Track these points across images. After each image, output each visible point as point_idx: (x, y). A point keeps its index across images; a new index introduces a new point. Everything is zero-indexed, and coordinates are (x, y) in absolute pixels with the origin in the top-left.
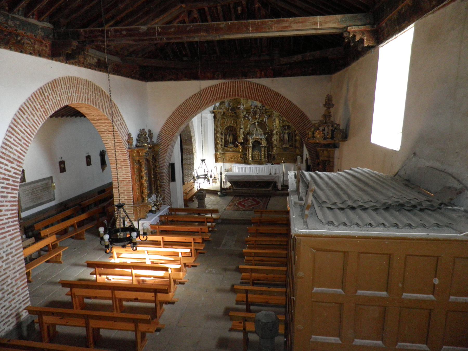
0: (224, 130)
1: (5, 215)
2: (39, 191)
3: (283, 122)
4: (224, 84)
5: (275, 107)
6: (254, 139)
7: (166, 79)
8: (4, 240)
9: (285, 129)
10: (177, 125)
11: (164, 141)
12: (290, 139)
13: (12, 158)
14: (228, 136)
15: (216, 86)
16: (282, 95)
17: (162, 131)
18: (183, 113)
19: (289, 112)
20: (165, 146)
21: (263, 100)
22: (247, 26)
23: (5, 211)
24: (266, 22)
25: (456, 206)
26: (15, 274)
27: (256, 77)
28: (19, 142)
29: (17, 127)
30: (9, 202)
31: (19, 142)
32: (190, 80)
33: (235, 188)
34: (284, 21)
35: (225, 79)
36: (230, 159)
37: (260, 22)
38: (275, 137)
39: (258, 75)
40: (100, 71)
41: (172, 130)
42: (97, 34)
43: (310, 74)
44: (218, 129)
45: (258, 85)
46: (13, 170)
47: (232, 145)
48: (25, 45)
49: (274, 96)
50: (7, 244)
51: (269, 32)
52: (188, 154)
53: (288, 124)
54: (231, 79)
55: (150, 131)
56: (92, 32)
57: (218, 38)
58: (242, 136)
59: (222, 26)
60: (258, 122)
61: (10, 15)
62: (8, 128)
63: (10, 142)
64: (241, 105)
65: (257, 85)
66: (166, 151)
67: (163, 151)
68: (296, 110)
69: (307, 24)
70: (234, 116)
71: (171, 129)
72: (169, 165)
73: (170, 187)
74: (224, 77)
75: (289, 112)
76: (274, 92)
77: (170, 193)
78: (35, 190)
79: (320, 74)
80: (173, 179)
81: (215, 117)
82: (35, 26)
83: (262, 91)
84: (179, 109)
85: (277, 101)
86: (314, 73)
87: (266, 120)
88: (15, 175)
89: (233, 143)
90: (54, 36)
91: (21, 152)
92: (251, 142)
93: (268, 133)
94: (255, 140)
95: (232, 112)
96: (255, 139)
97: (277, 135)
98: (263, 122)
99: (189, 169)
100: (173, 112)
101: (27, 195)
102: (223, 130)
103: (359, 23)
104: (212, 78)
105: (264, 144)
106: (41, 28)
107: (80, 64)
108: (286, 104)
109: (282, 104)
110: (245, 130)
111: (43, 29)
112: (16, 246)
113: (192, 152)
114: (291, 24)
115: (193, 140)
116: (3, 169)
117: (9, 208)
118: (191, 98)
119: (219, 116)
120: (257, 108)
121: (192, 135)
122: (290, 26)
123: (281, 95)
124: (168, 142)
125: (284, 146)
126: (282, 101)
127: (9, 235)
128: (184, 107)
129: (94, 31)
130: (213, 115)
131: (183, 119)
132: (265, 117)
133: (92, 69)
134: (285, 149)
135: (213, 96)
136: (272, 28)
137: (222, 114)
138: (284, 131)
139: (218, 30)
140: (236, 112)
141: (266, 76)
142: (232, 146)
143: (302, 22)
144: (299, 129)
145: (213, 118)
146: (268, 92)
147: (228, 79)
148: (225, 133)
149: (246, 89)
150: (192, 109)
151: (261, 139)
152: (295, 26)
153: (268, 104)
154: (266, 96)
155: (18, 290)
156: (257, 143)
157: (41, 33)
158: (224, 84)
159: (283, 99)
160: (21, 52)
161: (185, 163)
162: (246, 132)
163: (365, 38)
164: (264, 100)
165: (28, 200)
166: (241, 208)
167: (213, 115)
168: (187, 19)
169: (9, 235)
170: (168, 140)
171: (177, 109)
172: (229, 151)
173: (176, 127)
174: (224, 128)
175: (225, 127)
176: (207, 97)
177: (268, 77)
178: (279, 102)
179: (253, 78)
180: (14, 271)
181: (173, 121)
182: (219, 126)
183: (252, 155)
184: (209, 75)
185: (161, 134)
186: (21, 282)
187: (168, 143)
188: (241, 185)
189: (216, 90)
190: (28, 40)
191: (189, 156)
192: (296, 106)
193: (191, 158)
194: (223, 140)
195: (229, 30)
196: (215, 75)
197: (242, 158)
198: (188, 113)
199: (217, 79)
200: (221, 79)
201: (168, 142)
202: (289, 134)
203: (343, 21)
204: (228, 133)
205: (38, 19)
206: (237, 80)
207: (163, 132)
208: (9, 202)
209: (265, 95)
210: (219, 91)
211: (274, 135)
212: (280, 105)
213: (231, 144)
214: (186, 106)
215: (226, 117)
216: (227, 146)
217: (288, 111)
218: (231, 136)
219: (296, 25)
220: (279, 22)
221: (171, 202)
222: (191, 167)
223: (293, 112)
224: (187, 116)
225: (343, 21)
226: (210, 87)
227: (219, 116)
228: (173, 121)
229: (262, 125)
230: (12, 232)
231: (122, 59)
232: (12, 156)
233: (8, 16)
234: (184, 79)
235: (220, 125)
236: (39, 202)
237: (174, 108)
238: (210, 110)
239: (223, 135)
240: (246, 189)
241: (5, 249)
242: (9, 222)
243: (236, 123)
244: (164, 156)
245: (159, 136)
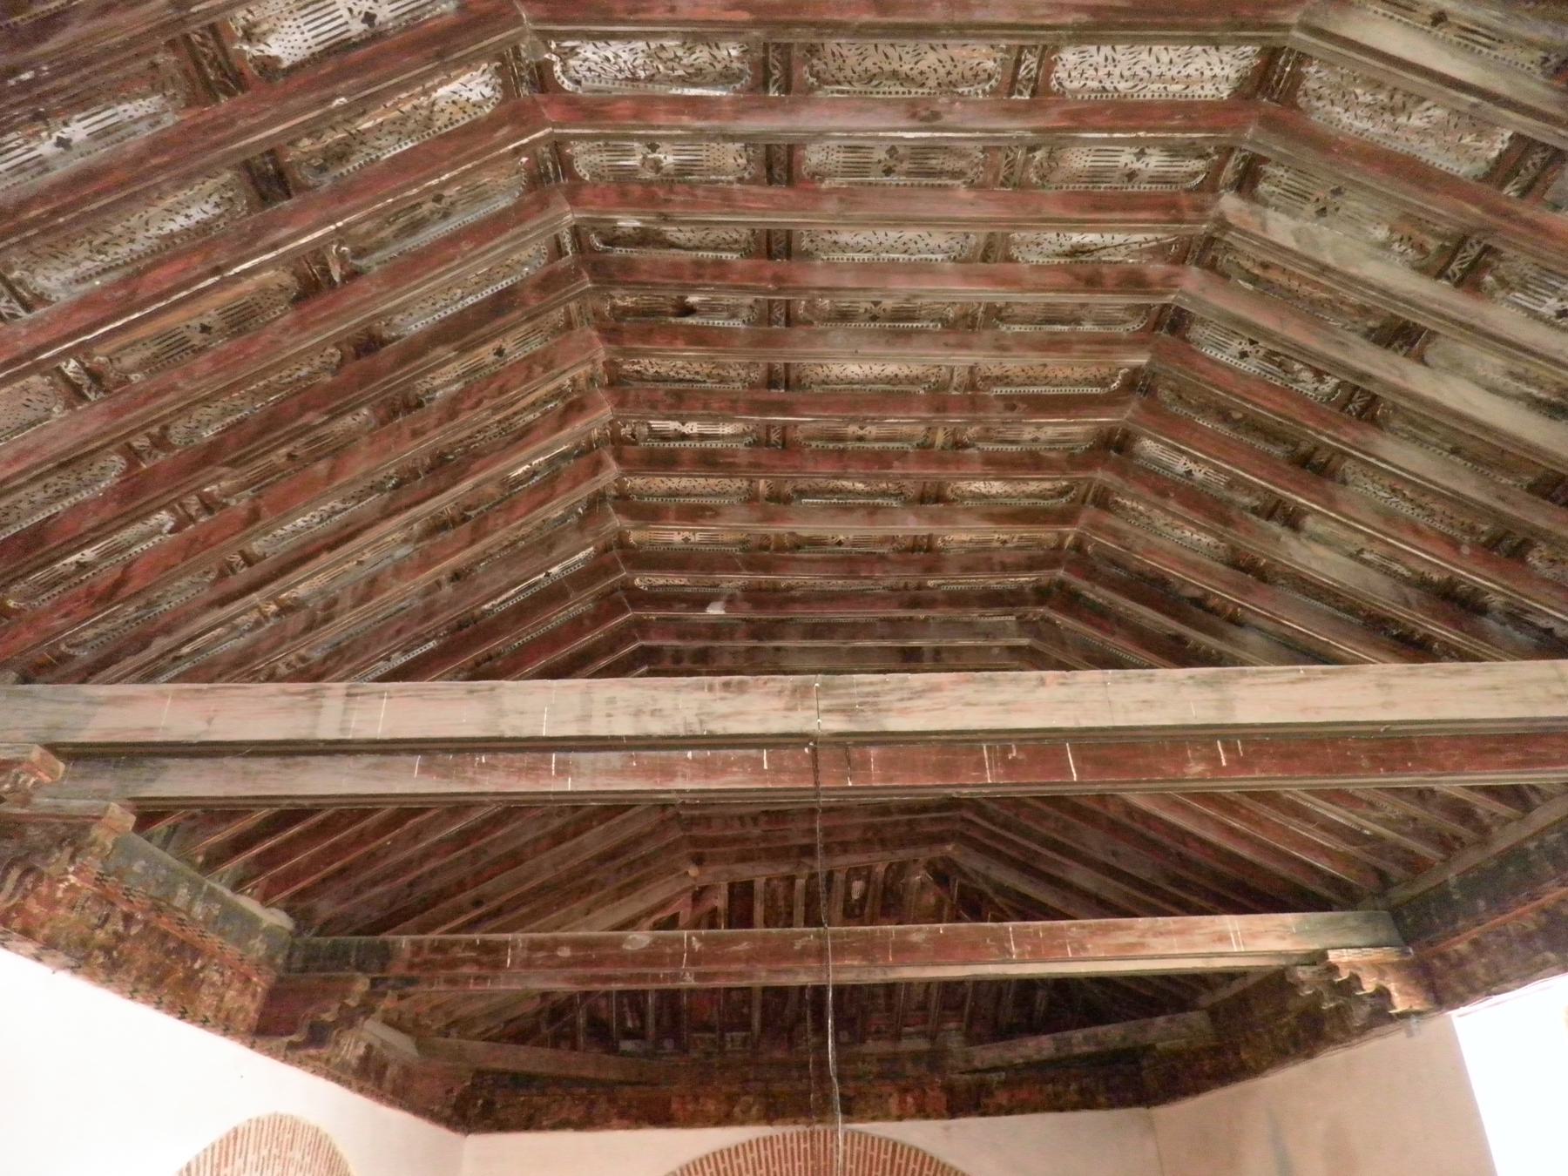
15: (736, 1151)
22: (1001, 940)
24: (1062, 929)
27: (887, 1117)
32: (639, 1127)
34: (1119, 928)
37: (1045, 929)
40: (361, 1090)
42: (461, 955)
43: (1075, 1107)
45: (895, 1145)
51: (1073, 960)
54: (795, 1123)
56: (440, 948)
57: (878, 976)
59: (916, 938)
61: (208, 882)
69: (1198, 939)
74: (771, 1114)
79: (1111, 1106)
82: (253, 921)
86: (1087, 1101)
90: (290, 956)
103: (1356, 941)
104: (725, 1119)
106: (264, 931)
111: (271, 933)
114: (1142, 936)
122: (1142, 945)
129: (454, 944)
133: (347, 1084)
136: (1084, 948)
139: (905, 951)
141: (923, 1112)
143: (1180, 932)
152: (1159, 945)
157: (258, 946)
163: (1392, 987)
168: (686, 914)
177: (927, 1117)
179: (874, 1119)
195: (942, 951)
199: (742, 1123)
200: (757, 1121)
203: (1305, 932)
205: (265, 899)
206: (818, 1127)
219: (1161, 940)
220: (1105, 931)
225: (1305, 932)
231: (419, 1046)
233: (200, 886)
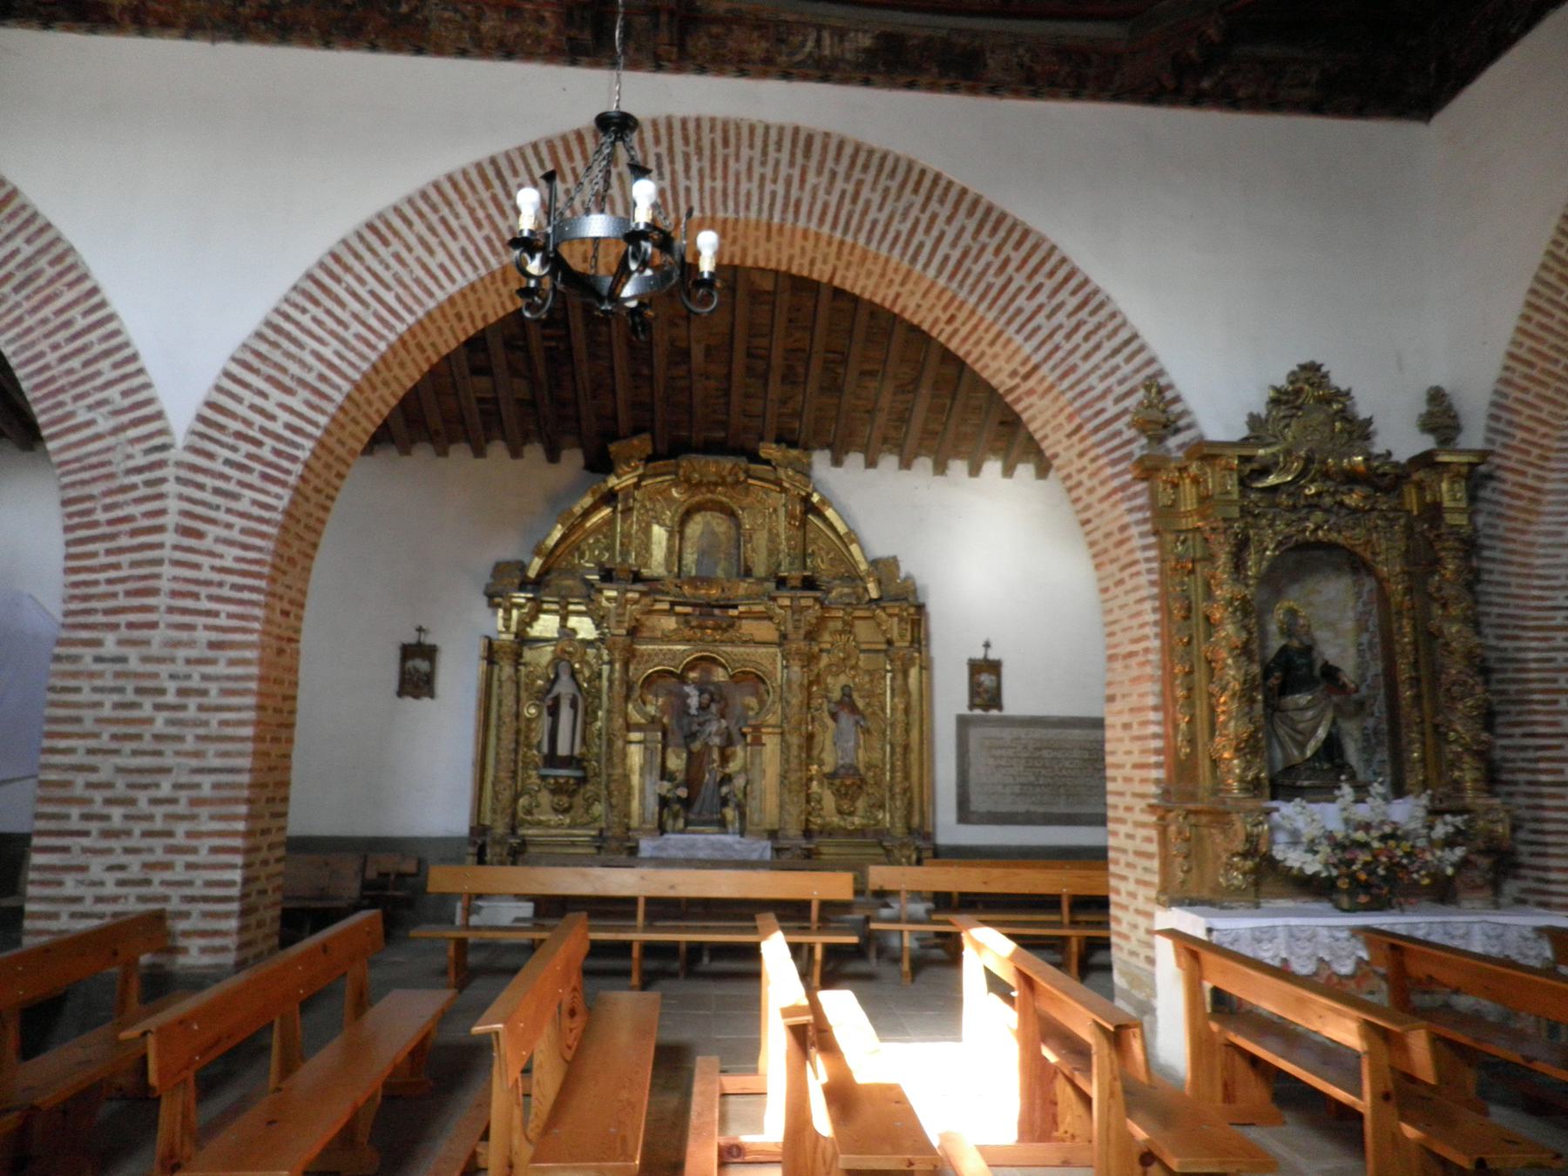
1: (211, 554)
2: (1067, 764)
8: (184, 635)
13: (293, 377)
23: (218, 540)
25: (144, 1059)
26: (197, 778)
28: (339, 330)
29: (338, 280)
30: (242, 515)
31: (339, 330)
40: (911, 86)
46: (284, 417)
48: (433, 25)
50: (193, 653)
62: (301, 279)
63: (297, 324)
78: (1045, 753)
88: (288, 434)
91: (336, 361)
101: (1003, 763)
107: (744, 66)
112: (228, 678)
116: (246, 403)
117: (234, 534)
124: (1545, 436)
127: (206, 628)
155: (193, 842)
160: (419, 51)
165: (1005, 786)
169: (206, 628)
180: (194, 763)
186: (212, 818)
187: (1545, 442)
190: (444, 9)
201: (1545, 436)
208: (242, 515)
230: (222, 621)
232: (294, 368)
236: (1061, 808)
241: (180, 668)
242: (220, 584)
244: (1528, 538)
245: (1498, 408)
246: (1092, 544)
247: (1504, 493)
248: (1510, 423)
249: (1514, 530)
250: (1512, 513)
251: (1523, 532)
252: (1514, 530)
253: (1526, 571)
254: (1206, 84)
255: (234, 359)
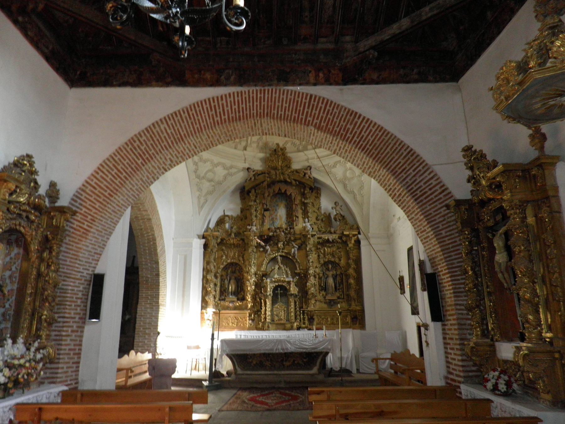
0: (220, 270)
3: (325, 256)
4: (240, 95)
5: (350, 138)
6: (275, 282)
7: (114, 83)
9: (328, 269)
10: (124, 174)
11: (84, 209)
12: (338, 285)
14: (226, 282)
16: (363, 115)
17: (84, 188)
18: (141, 150)
19: (381, 149)
20: (86, 223)
21: (322, 124)
27: (308, 83)
33: (239, 371)
35: (241, 85)
36: (228, 324)
38: (312, 281)
39: (312, 80)
41: (111, 185)
43: (416, 81)
44: (210, 266)
45: (311, 96)
47: (234, 297)
49: (346, 116)
52: (148, 306)
53: (333, 260)
54: (256, 86)
55: (53, 185)
58: (253, 279)
60: (281, 256)
64: (252, 225)
65: (308, 97)
66: (87, 235)
67: (78, 233)
68: (395, 144)
70: (240, 245)
71: (109, 183)
72: (88, 277)
73: (81, 336)
74: (241, 81)
75: (381, 149)
76: (345, 109)
77: (80, 354)
79: (436, 81)
80: (95, 312)
81: (206, 246)
83: (321, 108)
84: (135, 142)
85: (352, 126)
87: (296, 252)
89: (236, 293)
92: (271, 289)
93: (299, 274)
94: (277, 284)
95: (237, 237)
96: (277, 282)
97: (315, 276)
98: (290, 255)
99: (147, 337)
100: (120, 148)
102: (219, 271)
104: (216, 83)
105: (293, 289)
108: (372, 133)
109: (365, 132)
110: (258, 269)
113: (158, 302)
115: (161, 279)
116: (438, 189)
118: (165, 120)
119: (213, 243)
120: (280, 231)
121: (160, 270)
123: (360, 116)
124: (95, 213)
125: (329, 297)
126: (364, 126)
128: (147, 137)
130: (203, 241)
131: (139, 162)
132: (294, 247)
134: (330, 302)
135: (215, 116)
137: (219, 240)
138: (327, 273)
140: (243, 237)
141: (328, 82)
142: (234, 298)
144: (407, 182)
145: (202, 247)
146: (333, 109)
147: (249, 86)
148: (222, 276)
149: (286, 103)
150: (163, 142)
151: (289, 283)
153: (334, 132)
154: (329, 116)
156: (280, 290)
158: (240, 95)
159: (366, 123)
161: (140, 326)
162: (261, 273)
164: (325, 125)
166: (259, 407)
167: (203, 241)
170: (96, 209)
171: (131, 141)
172: (228, 308)
173: (121, 179)
174: (222, 266)
175: (223, 264)
176: (200, 117)
177: (331, 84)
178: (358, 129)
181: (116, 165)
182: (213, 261)
183: (272, 311)
184: (209, 77)
185: (82, 195)
187: (95, 215)
188: (254, 362)
189: (223, 104)
191: (149, 310)
192: (395, 137)
193: (154, 314)
194: (218, 289)
196: (221, 76)
197: (251, 319)
198: (154, 149)
199: (225, 85)
200: (234, 84)
201: (95, 213)
202: (335, 277)
204: (227, 275)
206: (266, 88)
207: (88, 191)
209: (327, 115)
210: (227, 106)
211: (310, 277)
212: (360, 133)
213: (232, 295)
214: (151, 136)
215: (226, 247)
216: (224, 300)
217: (377, 145)
218: (232, 281)
221: (77, 379)
222: (152, 334)
223: (390, 147)
224: (150, 155)
226: (209, 101)
227: (213, 243)
228: (116, 165)
229: (288, 260)
234: (154, 83)
235: (215, 260)
237: (122, 140)
238: (199, 234)
239: (219, 279)
240: (263, 372)
243: (243, 258)
244: (79, 246)
245: (76, 197)
246: (108, 239)
247: (72, 228)
248: (81, 204)
249: (73, 241)
250: (74, 235)
251: (78, 243)
252: (73, 241)
253: (75, 257)
254: (20, 19)
255: (335, 104)
